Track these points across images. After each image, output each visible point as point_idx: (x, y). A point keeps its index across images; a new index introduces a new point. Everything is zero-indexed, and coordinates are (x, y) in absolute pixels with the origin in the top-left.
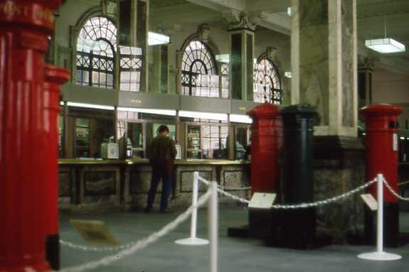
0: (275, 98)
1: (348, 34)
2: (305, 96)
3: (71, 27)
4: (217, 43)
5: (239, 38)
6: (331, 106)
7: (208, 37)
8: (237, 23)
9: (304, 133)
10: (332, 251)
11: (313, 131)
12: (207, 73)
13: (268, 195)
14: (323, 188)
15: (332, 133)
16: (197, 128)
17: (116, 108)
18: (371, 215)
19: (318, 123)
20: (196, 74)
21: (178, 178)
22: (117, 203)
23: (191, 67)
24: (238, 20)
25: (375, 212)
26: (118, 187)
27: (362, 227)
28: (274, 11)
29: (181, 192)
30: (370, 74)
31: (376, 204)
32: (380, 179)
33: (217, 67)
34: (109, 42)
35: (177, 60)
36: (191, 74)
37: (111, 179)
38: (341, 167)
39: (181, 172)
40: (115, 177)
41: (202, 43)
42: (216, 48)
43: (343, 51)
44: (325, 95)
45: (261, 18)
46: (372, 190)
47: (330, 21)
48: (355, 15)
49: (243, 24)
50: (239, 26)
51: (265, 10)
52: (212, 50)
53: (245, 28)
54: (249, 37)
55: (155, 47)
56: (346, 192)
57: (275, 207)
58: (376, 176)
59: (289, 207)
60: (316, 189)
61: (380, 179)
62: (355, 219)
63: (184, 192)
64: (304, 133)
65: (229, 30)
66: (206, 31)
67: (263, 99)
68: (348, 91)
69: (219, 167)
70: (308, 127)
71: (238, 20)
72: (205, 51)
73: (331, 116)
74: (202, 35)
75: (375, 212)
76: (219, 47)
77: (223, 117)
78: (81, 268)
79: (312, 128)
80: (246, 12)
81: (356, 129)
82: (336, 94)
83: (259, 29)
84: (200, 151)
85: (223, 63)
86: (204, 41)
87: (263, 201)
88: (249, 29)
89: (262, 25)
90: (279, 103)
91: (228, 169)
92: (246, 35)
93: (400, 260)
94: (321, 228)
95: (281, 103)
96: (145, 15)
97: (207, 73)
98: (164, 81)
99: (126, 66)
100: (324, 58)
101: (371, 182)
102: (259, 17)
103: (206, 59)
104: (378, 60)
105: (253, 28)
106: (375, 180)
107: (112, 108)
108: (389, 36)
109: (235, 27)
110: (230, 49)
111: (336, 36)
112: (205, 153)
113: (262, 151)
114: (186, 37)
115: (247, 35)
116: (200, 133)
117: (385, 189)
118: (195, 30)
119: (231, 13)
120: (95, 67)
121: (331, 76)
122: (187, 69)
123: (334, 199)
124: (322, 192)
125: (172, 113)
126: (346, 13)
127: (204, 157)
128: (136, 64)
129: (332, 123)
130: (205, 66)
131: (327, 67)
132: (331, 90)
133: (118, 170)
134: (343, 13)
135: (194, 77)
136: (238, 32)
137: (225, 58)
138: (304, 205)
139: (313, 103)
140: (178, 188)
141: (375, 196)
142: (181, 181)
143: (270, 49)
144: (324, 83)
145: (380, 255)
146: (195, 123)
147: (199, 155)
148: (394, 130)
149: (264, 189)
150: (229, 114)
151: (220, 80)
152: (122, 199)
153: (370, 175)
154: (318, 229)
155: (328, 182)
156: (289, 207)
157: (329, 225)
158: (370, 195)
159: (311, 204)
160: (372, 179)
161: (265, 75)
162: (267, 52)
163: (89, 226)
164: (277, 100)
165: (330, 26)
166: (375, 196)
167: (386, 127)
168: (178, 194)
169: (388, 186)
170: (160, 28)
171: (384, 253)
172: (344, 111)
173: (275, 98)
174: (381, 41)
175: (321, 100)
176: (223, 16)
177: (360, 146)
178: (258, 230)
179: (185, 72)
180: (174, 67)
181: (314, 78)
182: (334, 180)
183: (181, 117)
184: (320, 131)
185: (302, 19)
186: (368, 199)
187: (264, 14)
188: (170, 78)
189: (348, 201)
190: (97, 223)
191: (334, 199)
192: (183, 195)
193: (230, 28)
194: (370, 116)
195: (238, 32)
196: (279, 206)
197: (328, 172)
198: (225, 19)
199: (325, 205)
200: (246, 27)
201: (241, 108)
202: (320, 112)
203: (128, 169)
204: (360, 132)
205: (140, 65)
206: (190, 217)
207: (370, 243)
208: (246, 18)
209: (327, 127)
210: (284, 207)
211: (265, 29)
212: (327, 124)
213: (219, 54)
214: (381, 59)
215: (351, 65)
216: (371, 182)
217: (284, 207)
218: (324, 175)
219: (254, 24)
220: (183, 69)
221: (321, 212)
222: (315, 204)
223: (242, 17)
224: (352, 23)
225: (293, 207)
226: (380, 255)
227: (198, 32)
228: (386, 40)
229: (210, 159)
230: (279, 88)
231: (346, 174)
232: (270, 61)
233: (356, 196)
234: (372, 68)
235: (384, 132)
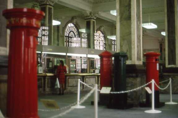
1: (139, 24)
2: (122, 49)
3: (63, 28)
4: (80, 24)
5: (89, 22)
6: (133, 52)
7: (76, 22)
8: (89, 16)
10: (135, 110)
11: (126, 63)
12: (75, 37)
13: (108, 88)
14: (130, 85)
15: (133, 63)
16: (74, 60)
17: (41, 52)
18: (148, 96)
19: (127, 59)
20: (71, 37)
21: (67, 80)
22: (43, 92)
23: (69, 34)
25: (151, 94)
26: (43, 85)
27: (145, 100)
28: (104, 12)
29: (68, 86)
31: (151, 91)
32: (153, 82)
33: (79, 34)
35: (63, 30)
36: (69, 37)
37: (40, 82)
38: (137, 76)
39: (68, 78)
40: (41, 81)
41: (73, 24)
42: (79, 26)
43: (137, 31)
44: (130, 49)
45: (99, 14)
46: (150, 86)
47: (132, 19)
48: (141, 16)
49: (47, 2)
50: (89, 17)
51: (100, 11)
52: (77, 27)
53: (48, 4)
54: (94, 22)
55: (54, 26)
56: (139, 87)
57: (111, 93)
58: (151, 80)
59: (117, 93)
60: (127, 85)
61: (153, 82)
62: (142, 97)
63: (70, 87)
65: (85, 19)
66: (75, 19)
67: (99, 47)
68: (139, 47)
69: (83, 77)
70: (124, 61)
71: (89, 15)
72: (75, 28)
73: (133, 56)
74: (73, 21)
75: (151, 94)
76: (80, 26)
77: (85, 56)
78: (56, 116)
79: (125, 61)
80: (92, 12)
81: (142, 62)
82: (134, 48)
83: (98, 19)
84: (76, 70)
85: (82, 33)
86: (74, 23)
87: (106, 90)
89: (99, 17)
91: (87, 77)
92: (92, 22)
93: (161, 113)
94: (129, 101)
96: (51, 14)
97: (75, 37)
98: (58, 40)
100: (130, 34)
101: (150, 83)
103: (75, 30)
104: (146, 31)
105: (95, 18)
106: (151, 82)
107: (40, 52)
108: (151, 22)
109: (88, 18)
110: (86, 27)
111: (134, 25)
112: (78, 71)
113: (105, 70)
114: (66, 23)
115: (93, 21)
116: (75, 62)
117: (155, 85)
118: (70, 19)
120: (70, 41)
121: (132, 40)
122: (67, 35)
123: (135, 89)
124: (129, 87)
125: (64, 54)
126: (138, 16)
127: (77, 72)
128: (46, 33)
129: (133, 59)
130: (74, 34)
131: (131, 37)
132: (133, 47)
133: (43, 78)
134: (137, 16)
135: (70, 38)
136: (89, 20)
137: (83, 31)
138: (123, 92)
139: (125, 51)
140: (67, 85)
141: (151, 88)
142: (68, 82)
143: (101, 27)
144: (130, 43)
145: (153, 111)
146: (73, 58)
147: (75, 72)
148: (157, 62)
149: (107, 85)
150: (87, 55)
151: (81, 40)
152: (44, 90)
153: (148, 80)
154: (128, 101)
155: (132, 82)
156: (117, 93)
157: (132, 100)
158: (148, 88)
159: (126, 92)
160: (150, 81)
161: (99, 37)
163: (48, 102)
165: (132, 21)
166: (151, 88)
167: (154, 61)
168: (67, 87)
169: (156, 84)
170: (56, 18)
171: (155, 110)
172: (138, 54)
174: (147, 24)
176: (83, 14)
177: (144, 68)
178: (106, 102)
179: (66, 36)
180: (62, 34)
181: (126, 41)
182: (134, 82)
183: (68, 56)
184: (128, 62)
185: (121, 18)
186: (148, 89)
188: (60, 39)
189: (139, 90)
190: (51, 101)
191: (135, 89)
192: (69, 88)
193: (86, 19)
194: (148, 57)
195: (89, 20)
196: (113, 93)
197: (132, 79)
199: (131, 92)
201: (92, 52)
202: (128, 54)
203: (47, 78)
204: (143, 63)
207: (148, 105)
210: (115, 93)
211: (99, 18)
212: (131, 60)
213: (81, 29)
214: (147, 31)
215: (140, 36)
216: (150, 83)
217: (115, 93)
218: (129, 80)
219: (95, 17)
220: (66, 35)
221: (129, 94)
222: (127, 91)
223: (90, 14)
224: (140, 19)
225: (118, 93)
226: (153, 111)
227: (72, 20)
228: (150, 23)
229: (80, 73)
231: (139, 80)
232: (101, 31)
233: (143, 89)
235: (153, 63)
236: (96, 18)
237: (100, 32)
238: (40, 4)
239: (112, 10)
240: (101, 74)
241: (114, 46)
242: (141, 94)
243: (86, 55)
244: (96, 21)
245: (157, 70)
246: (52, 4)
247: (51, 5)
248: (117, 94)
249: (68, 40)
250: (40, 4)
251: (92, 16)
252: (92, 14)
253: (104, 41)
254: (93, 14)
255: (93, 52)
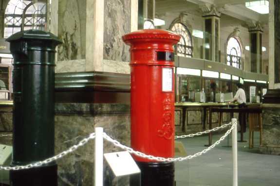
0: (187, 53)
8: (209, 12)
9: (37, 70)
24: (210, 10)
30: (261, 35)
34: (28, 6)
54: (217, 21)
64: (37, 70)
66: (185, 16)
71: (210, 10)
88: (216, 16)
90: (190, 57)
95: (192, 57)
99: (18, 18)
102: (223, 8)
106: (91, 136)
107: (265, 82)
109: (208, 14)
110: (204, 29)
119: (205, 5)
125: (254, 81)
136: (255, 32)
143: (182, 14)
150: (219, 73)
160: (87, 135)
162: (180, 17)
164: (188, 55)
167: (154, 60)
173: (187, 53)
175: (78, 26)
187: (226, 6)
197: (79, 119)
198: (201, 9)
200: (214, 14)
205: (25, 19)
206: (230, 137)
208: (215, 9)
209: (84, 60)
212: (84, 57)
219: (219, 12)
225: (45, 162)
230: (190, 45)
232: (182, 24)
234: (262, 30)
235: (151, 66)
236: (220, 14)
237: (180, 25)
238: (249, 29)
239: (247, 1)
240: (15, 102)
241: (187, 44)
242: (76, 177)
243: (230, 76)
244: (220, 20)
245: (163, 94)
246: (219, 15)
247: (216, 16)
248: (21, 171)
249: (185, 52)
250: (250, 30)
251: (259, 26)
252: (260, 25)
253: (190, 42)
254: (216, 8)
255: (210, 67)
